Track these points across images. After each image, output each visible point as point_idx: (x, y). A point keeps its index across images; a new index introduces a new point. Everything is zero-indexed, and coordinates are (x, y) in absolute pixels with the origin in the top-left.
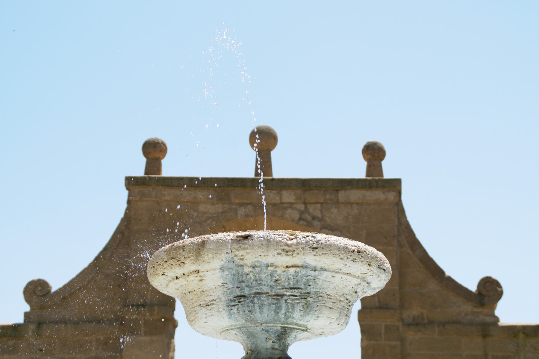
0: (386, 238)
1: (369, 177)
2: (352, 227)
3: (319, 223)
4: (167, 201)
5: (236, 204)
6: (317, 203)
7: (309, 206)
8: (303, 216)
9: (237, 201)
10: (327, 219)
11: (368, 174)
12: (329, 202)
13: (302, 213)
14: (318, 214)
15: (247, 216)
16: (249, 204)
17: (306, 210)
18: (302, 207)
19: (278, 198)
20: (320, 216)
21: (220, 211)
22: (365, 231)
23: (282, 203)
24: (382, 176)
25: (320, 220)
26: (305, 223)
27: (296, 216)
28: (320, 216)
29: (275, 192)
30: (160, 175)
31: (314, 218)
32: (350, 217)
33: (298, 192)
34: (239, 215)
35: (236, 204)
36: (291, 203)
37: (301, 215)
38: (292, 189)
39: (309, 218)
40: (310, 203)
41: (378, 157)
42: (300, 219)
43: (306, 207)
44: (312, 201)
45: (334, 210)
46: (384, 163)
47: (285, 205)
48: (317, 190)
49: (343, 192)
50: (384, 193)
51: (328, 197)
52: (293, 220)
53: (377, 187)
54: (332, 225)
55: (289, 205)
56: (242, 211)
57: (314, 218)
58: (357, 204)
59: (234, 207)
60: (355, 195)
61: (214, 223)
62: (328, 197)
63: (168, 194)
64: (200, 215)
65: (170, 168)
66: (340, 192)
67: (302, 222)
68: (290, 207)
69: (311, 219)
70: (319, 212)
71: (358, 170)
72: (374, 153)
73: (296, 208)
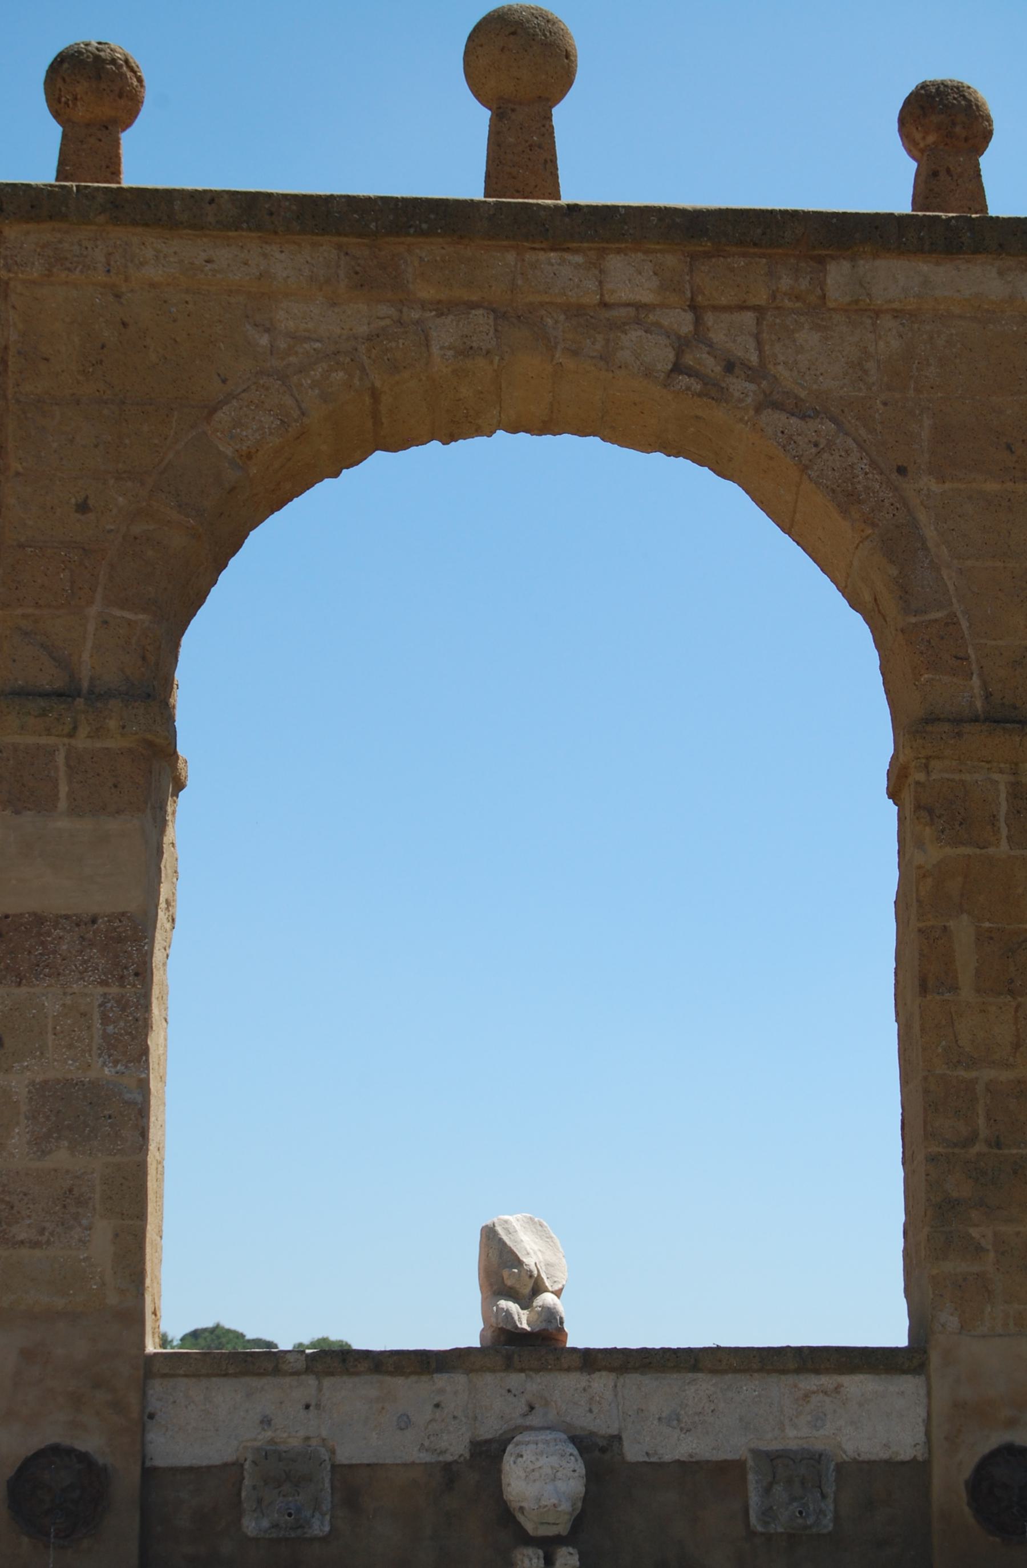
0: (1009, 447)
1: (490, 197)
2: (879, 404)
3: (753, 387)
4: (153, 285)
5: (423, 305)
6: (742, 308)
7: (709, 318)
8: (688, 360)
9: (426, 292)
10: (782, 371)
11: (923, 195)
12: (787, 303)
13: (681, 345)
14: (746, 350)
15: (467, 351)
16: (473, 306)
17: (700, 334)
18: (683, 322)
19: (591, 285)
20: (754, 358)
21: (363, 329)
22: (927, 422)
23: (604, 305)
24: (115, 173)
25: (755, 374)
26: (698, 387)
27: (662, 356)
28: (754, 358)
29: (579, 259)
30: (560, 199)
31: (730, 367)
32: (870, 365)
33: (671, 260)
34: (435, 350)
35: (423, 305)
36: (639, 306)
37: (679, 353)
38: (646, 252)
39: (712, 366)
40: (715, 308)
41: (966, 140)
42: (678, 368)
43: (698, 321)
44: (724, 301)
45: (808, 338)
46: (987, 162)
47: (614, 313)
48: (744, 255)
49: (846, 265)
50: (1001, 273)
51: (785, 282)
52: (648, 374)
53: (976, 251)
54: (803, 394)
55: (632, 311)
56: (445, 333)
57: (730, 367)
58: (897, 314)
59: (415, 315)
60: (894, 277)
61: (340, 376)
62: (785, 282)
63: (159, 259)
64: (282, 344)
65: (148, 159)
66: (832, 267)
67: (684, 380)
68: (638, 322)
69: (718, 369)
70: (752, 345)
71: (884, 182)
72: (944, 123)
73: (658, 325)
